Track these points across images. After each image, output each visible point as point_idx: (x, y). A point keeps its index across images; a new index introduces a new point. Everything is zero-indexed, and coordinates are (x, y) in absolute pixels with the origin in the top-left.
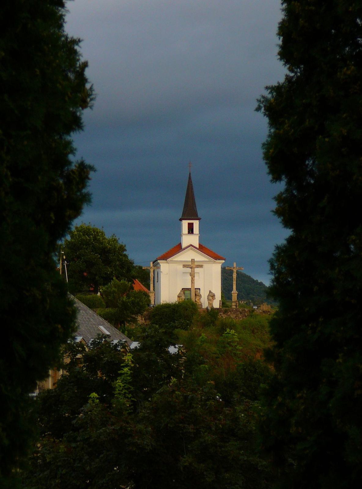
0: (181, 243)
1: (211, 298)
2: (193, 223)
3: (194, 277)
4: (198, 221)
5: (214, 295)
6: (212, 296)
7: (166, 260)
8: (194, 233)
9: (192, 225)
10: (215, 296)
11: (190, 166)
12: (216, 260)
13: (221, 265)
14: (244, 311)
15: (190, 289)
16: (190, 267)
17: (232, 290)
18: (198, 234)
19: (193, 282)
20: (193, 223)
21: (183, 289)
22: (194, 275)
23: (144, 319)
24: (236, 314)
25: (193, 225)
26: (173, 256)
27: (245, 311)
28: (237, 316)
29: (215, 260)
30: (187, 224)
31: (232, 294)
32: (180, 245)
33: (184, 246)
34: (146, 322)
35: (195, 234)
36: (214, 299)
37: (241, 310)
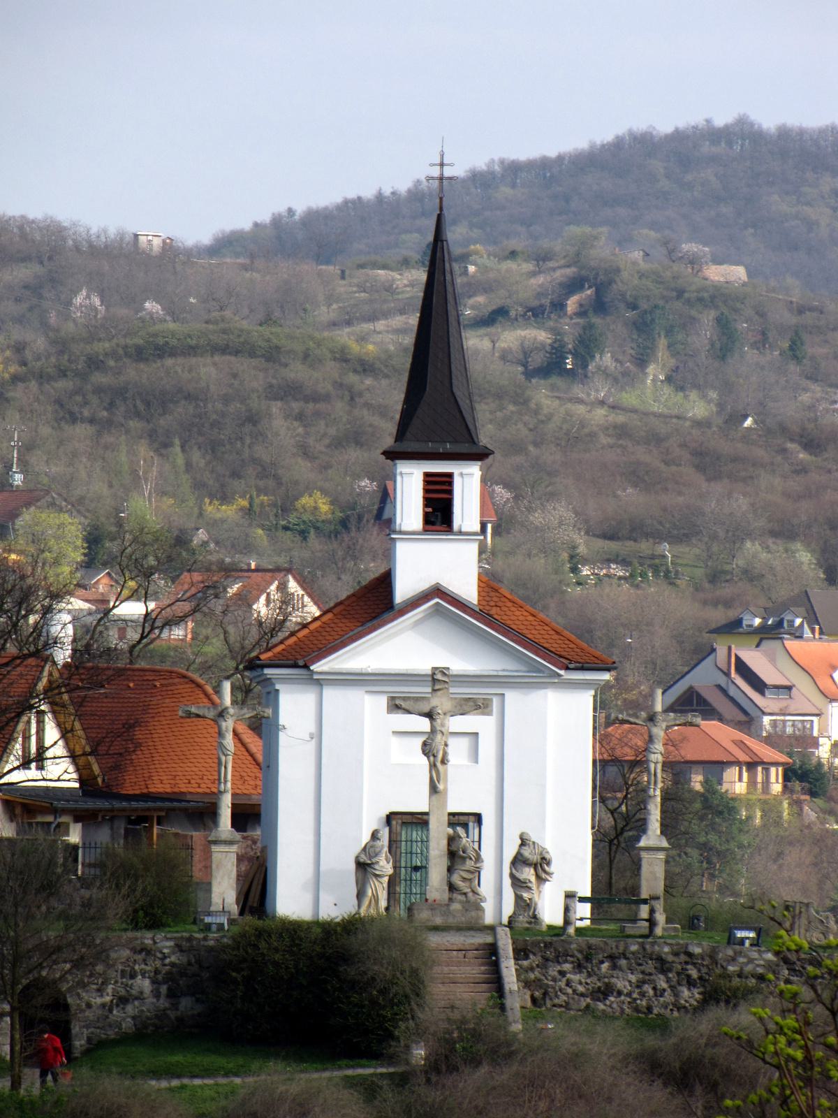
0: (390, 570)
1: (528, 874)
2: (450, 475)
3: (444, 762)
4: (479, 463)
5: (543, 858)
6: (535, 866)
7: (306, 667)
8: (456, 526)
9: (235, 765)
10: (548, 863)
11: (442, 165)
12: (567, 668)
13: (592, 692)
14: (683, 958)
15: (427, 814)
16: (426, 709)
17: (642, 827)
18: (475, 534)
19: (441, 787)
20: (450, 475)
21: (390, 818)
22: (445, 754)
23: (169, 989)
24: (643, 972)
25: (451, 483)
26: (344, 645)
27: (690, 955)
28: (644, 982)
29: (562, 672)
30: (421, 477)
31: (644, 855)
32: (385, 582)
33: (403, 589)
34: (175, 1006)
35: (460, 533)
36: (544, 876)
37: (666, 949)
